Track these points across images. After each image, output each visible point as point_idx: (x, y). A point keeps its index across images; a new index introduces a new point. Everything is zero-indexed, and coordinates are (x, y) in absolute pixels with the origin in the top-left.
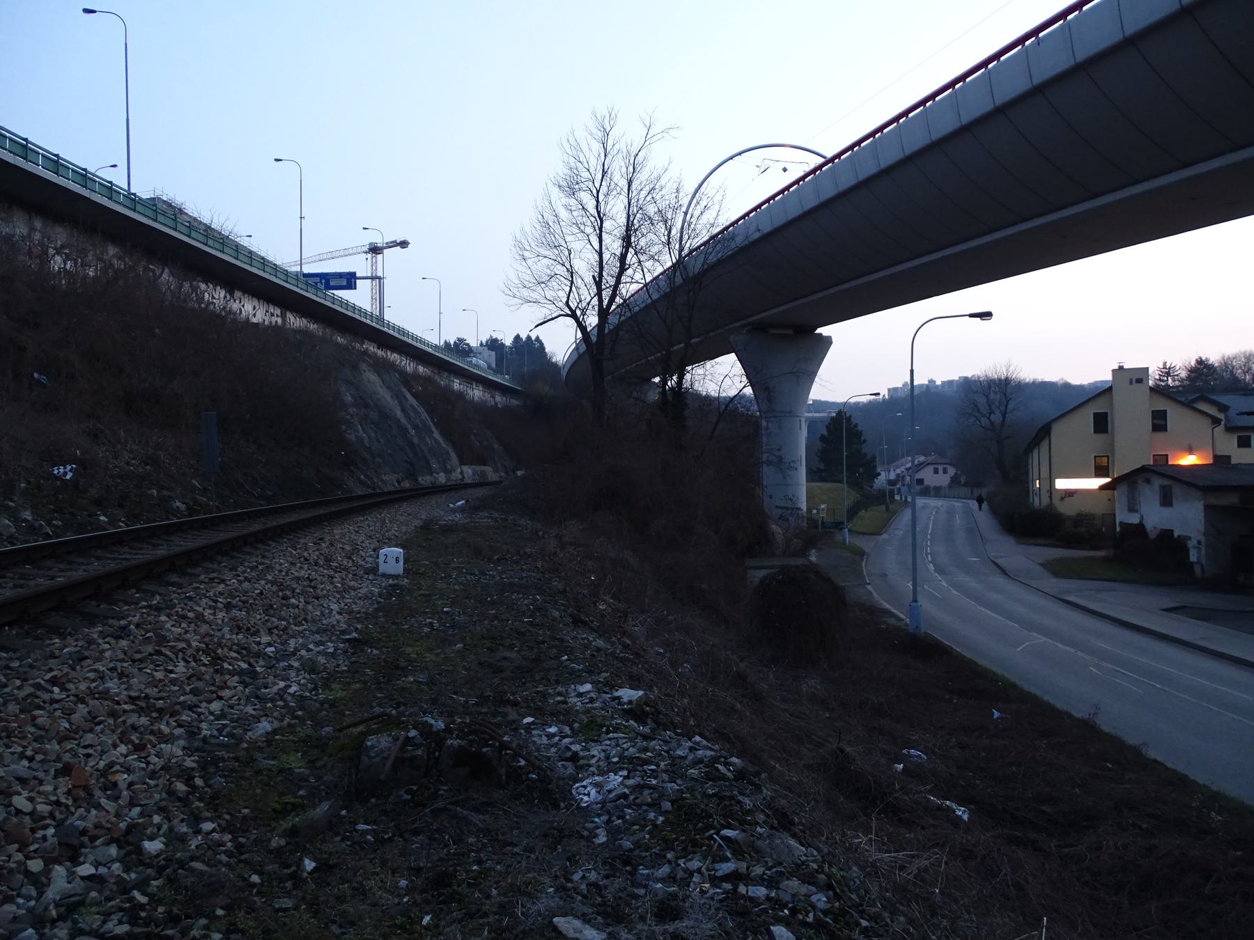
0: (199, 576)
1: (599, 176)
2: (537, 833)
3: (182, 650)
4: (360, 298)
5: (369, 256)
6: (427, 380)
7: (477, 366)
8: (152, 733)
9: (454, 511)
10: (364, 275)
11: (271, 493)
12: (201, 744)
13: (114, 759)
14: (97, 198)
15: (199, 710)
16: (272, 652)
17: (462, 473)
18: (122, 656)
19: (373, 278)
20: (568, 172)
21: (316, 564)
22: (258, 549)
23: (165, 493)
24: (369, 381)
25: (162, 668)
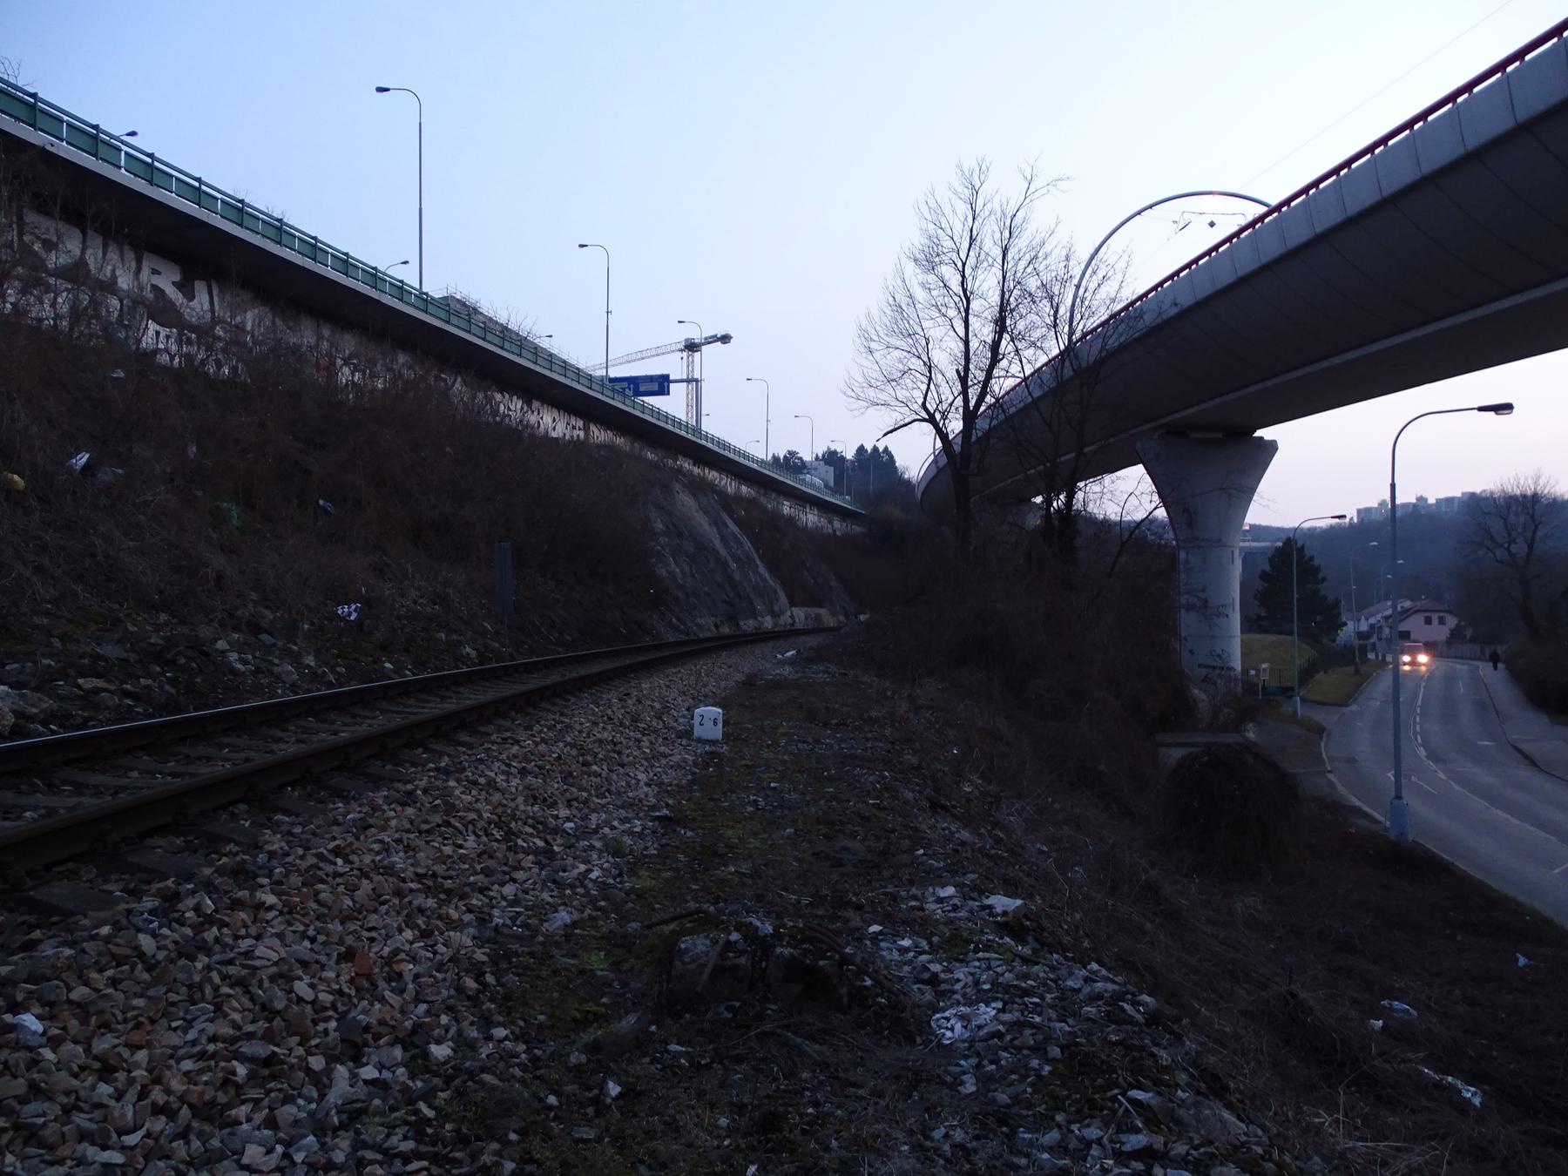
0: (490, 735)
3: (472, 822)
4: (673, 405)
5: (685, 354)
6: (751, 502)
7: (813, 486)
8: (440, 917)
9: (782, 663)
10: (679, 377)
12: (493, 934)
14: (387, 300)
16: (571, 829)
17: (792, 616)
19: (688, 381)
22: (556, 704)
25: (450, 842)
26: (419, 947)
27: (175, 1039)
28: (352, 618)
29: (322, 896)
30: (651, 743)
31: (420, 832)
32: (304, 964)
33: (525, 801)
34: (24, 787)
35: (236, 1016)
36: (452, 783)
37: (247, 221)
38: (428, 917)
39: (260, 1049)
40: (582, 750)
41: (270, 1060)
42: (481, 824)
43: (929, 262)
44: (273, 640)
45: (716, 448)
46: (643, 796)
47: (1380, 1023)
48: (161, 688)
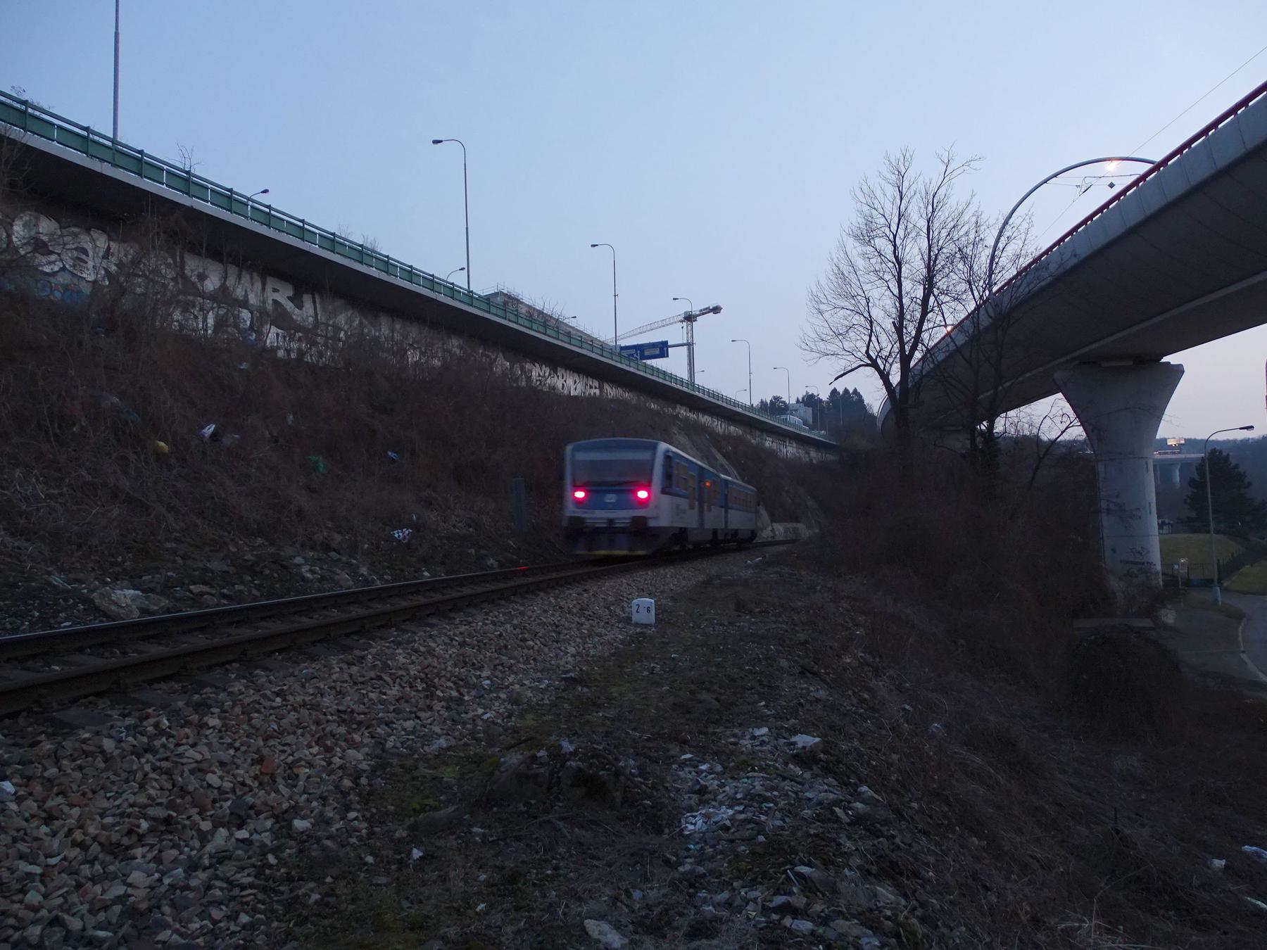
1: (896, 220)
2: (626, 851)
3: (400, 677)
4: (673, 365)
5: (685, 324)
6: (739, 440)
7: (793, 425)
14: (442, 298)
15: (394, 726)
21: (570, 612)
23: (483, 552)
25: (378, 690)
27: (105, 804)
29: (253, 722)
32: (222, 764)
35: (152, 792)
37: (338, 248)
39: (161, 813)
41: (168, 821)
43: (866, 236)
44: (338, 556)
45: (711, 399)
47: (1223, 862)
48: (250, 591)
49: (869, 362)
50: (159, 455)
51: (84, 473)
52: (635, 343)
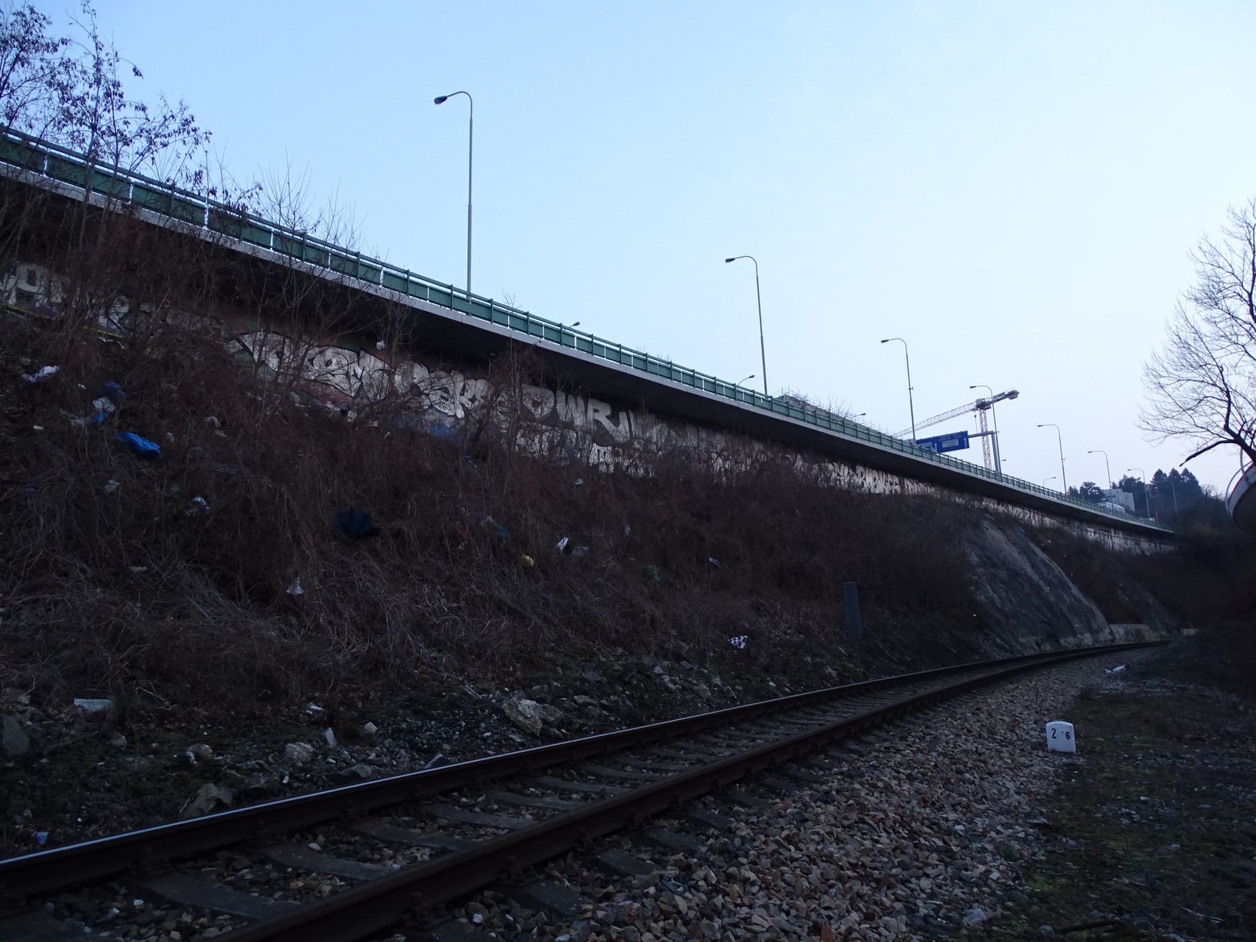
0: (873, 744)
3: (882, 820)
4: (973, 456)
5: (977, 413)
6: (1056, 532)
7: (1115, 512)
8: (875, 903)
9: (1114, 677)
10: (975, 433)
11: (909, 659)
12: (922, 923)
13: (851, 925)
16: (962, 831)
17: (1111, 633)
18: (833, 821)
19: (984, 434)
20: (1206, 282)
22: (918, 718)
23: (818, 660)
24: (993, 537)
25: (867, 837)
26: (867, 928)
28: (742, 647)
29: (787, 876)
30: (1011, 754)
31: (844, 827)
33: (918, 804)
34: (566, 775)
36: (857, 786)
37: (650, 367)
38: (866, 902)
40: (954, 761)
42: (889, 823)
44: (690, 666)
46: (1017, 804)
49: (1232, 438)
50: (526, 567)
51: (473, 587)
52: (932, 436)
